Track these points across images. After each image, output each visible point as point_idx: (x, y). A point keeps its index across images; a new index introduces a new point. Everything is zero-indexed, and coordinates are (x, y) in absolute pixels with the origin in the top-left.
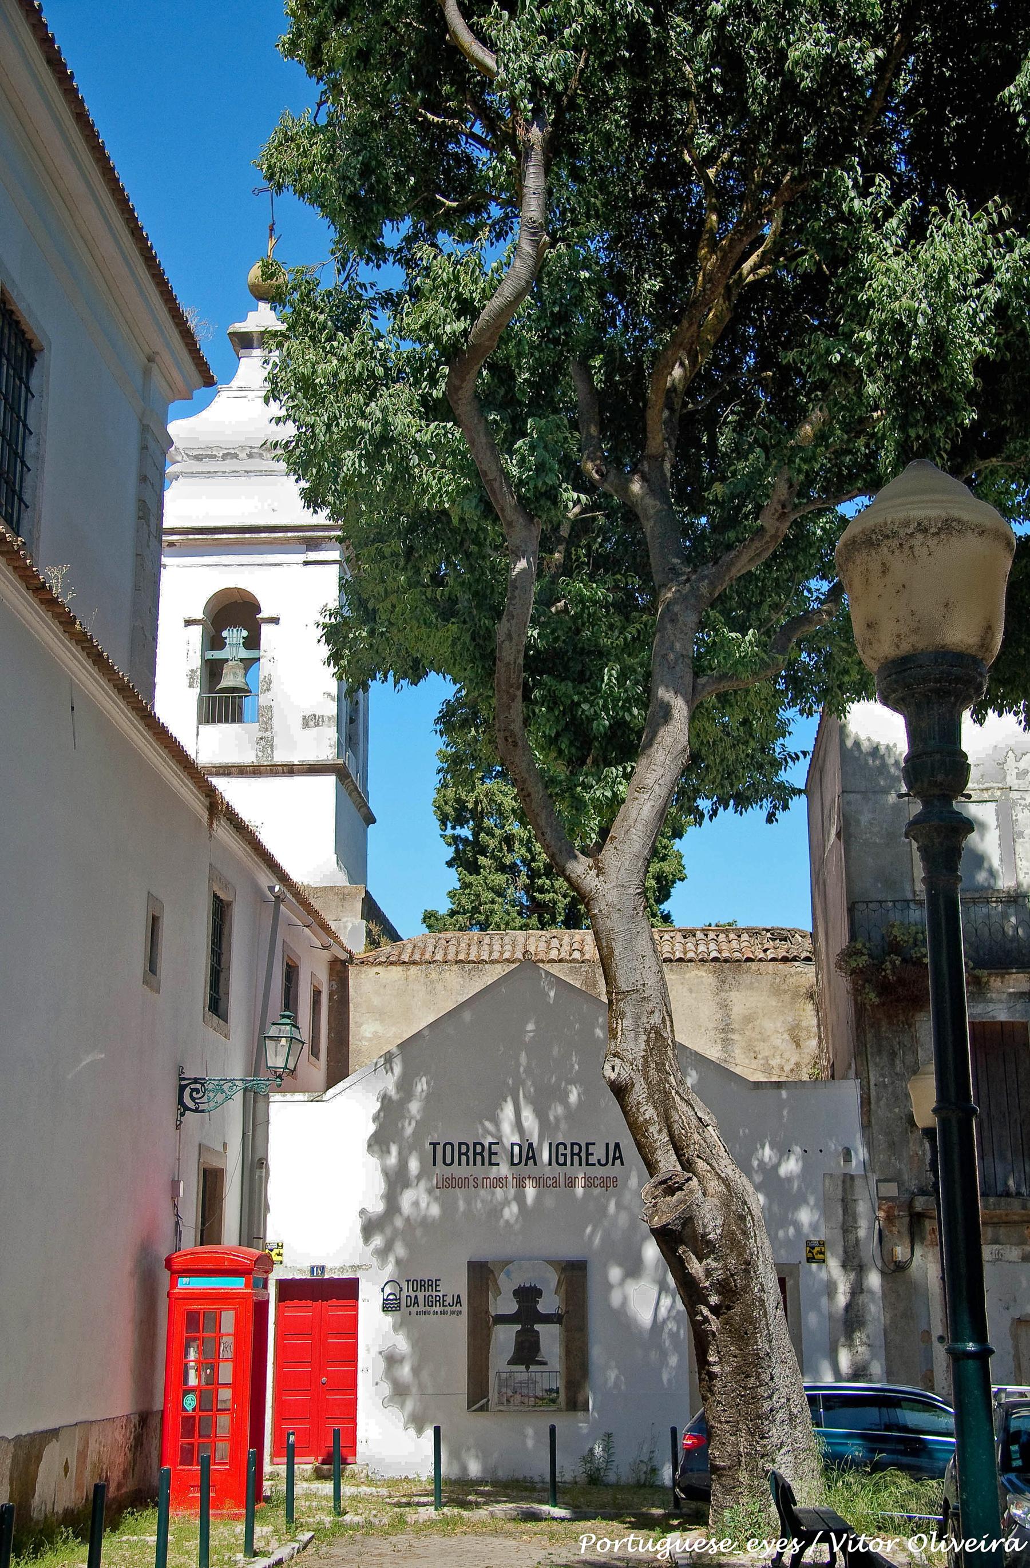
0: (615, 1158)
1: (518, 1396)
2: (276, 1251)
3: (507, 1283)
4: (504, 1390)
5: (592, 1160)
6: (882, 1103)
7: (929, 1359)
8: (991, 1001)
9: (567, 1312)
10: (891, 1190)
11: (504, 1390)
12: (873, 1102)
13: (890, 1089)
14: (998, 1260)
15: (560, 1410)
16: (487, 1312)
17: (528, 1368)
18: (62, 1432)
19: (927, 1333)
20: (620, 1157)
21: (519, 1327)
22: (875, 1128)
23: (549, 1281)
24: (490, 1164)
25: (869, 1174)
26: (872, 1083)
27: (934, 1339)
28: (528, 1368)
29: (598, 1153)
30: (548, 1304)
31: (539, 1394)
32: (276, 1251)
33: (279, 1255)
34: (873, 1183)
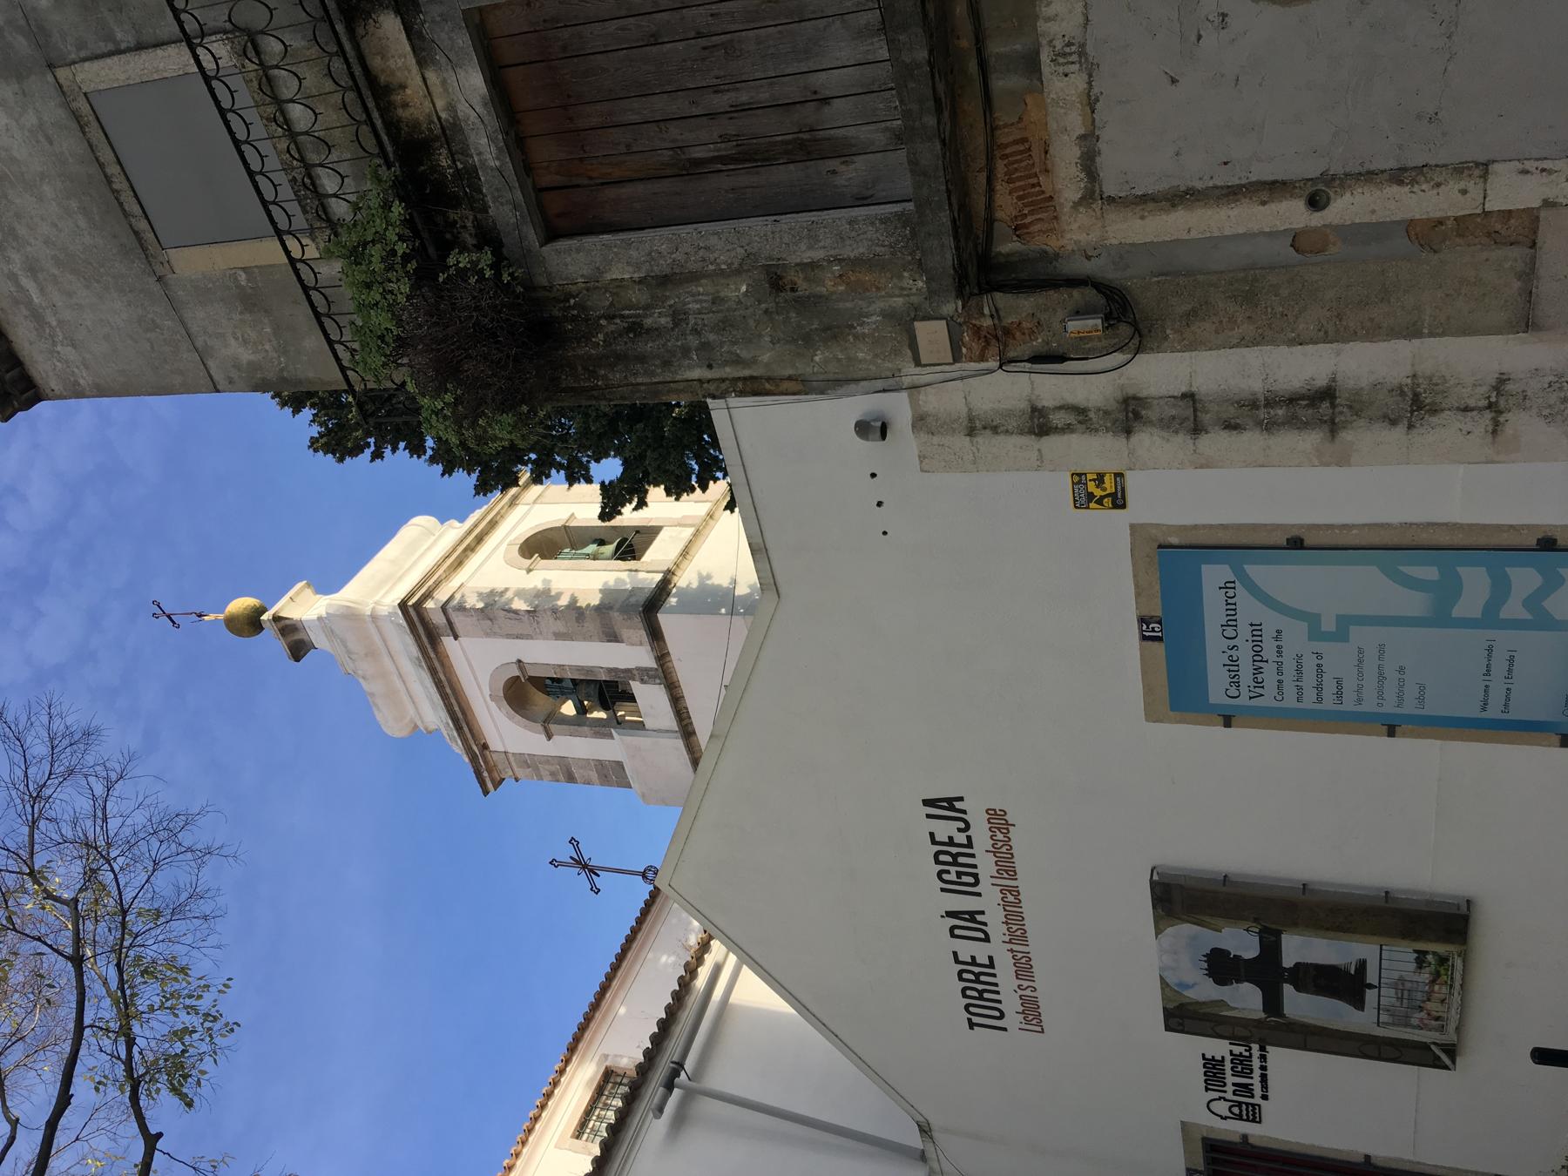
0: (973, 920)
1: (1429, 1005)
2: (1092, 487)
3: (1205, 990)
4: (1414, 1022)
5: (961, 838)
6: (744, 354)
7: (1375, 232)
8: (451, 107)
9: (1256, 920)
10: (932, 334)
11: (1414, 1022)
12: (747, 373)
13: (712, 337)
14: (1082, 53)
15: (1464, 956)
16: (1259, 1021)
17: (1371, 986)
18: (1532, 542)
19: (1297, 240)
20: (950, 800)
21: (1288, 989)
22: (802, 368)
23: (1192, 938)
24: (992, 965)
25: (907, 381)
26: (708, 374)
27: (1317, 219)
28: (1371, 986)
29: (945, 830)
30: (1242, 943)
31: (1425, 976)
32: (1092, 487)
33: (1100, 479)
34: (925, 376)
